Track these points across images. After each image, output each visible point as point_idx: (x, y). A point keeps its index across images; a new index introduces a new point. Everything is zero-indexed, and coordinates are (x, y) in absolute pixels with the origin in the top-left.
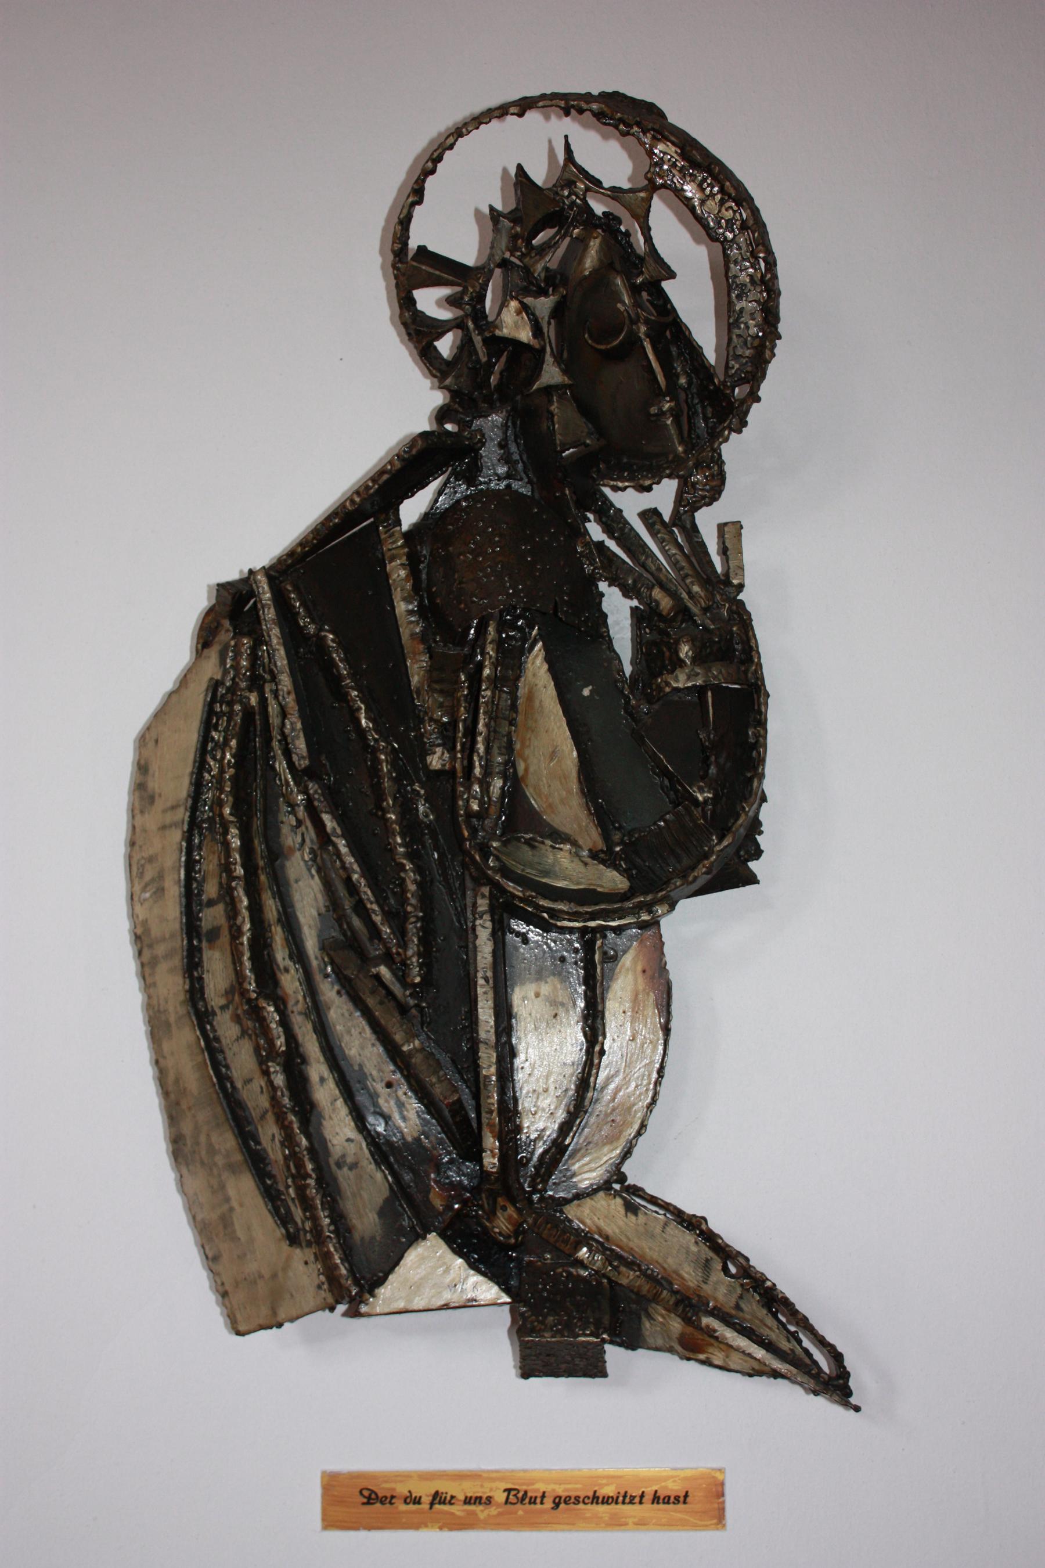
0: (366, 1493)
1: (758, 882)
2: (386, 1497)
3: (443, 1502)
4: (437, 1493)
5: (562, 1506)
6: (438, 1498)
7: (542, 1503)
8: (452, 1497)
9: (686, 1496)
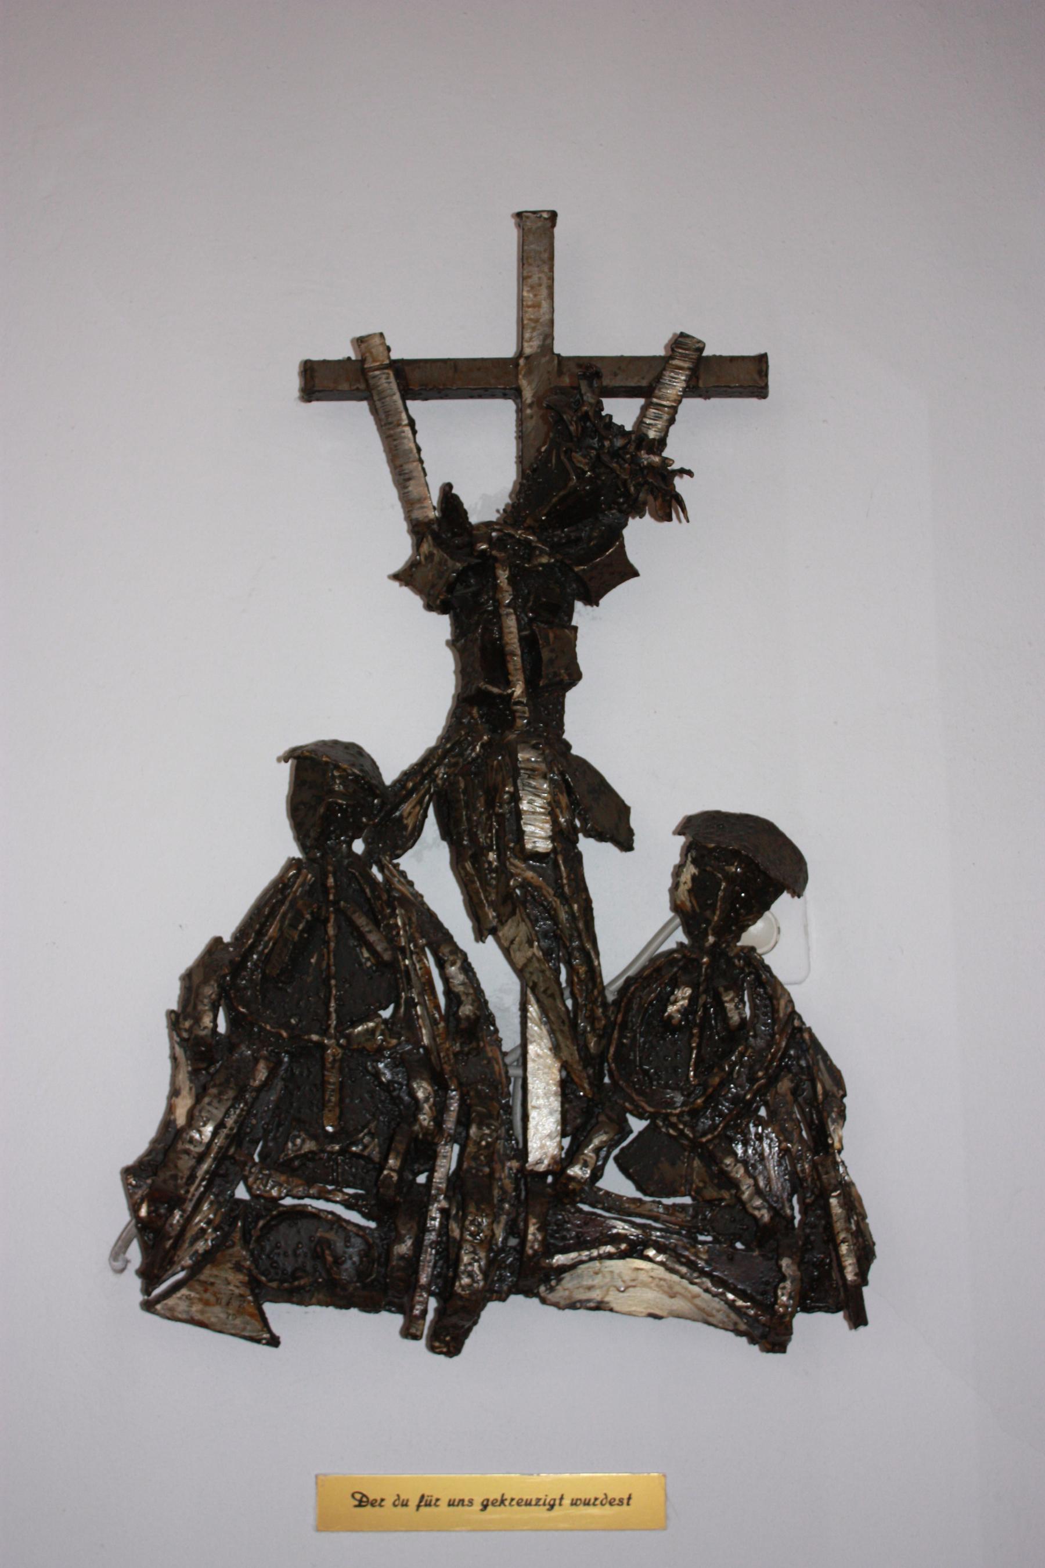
0: (358, 1496)
1: (636, 574)
2: (376, 1500)
3: (428, 1505)
4: (423, 1496)
5: (490, 1508)
6: (424, 1502)
7: (628, 1504)
8: (438, 1500)
9: (629, 1498)
